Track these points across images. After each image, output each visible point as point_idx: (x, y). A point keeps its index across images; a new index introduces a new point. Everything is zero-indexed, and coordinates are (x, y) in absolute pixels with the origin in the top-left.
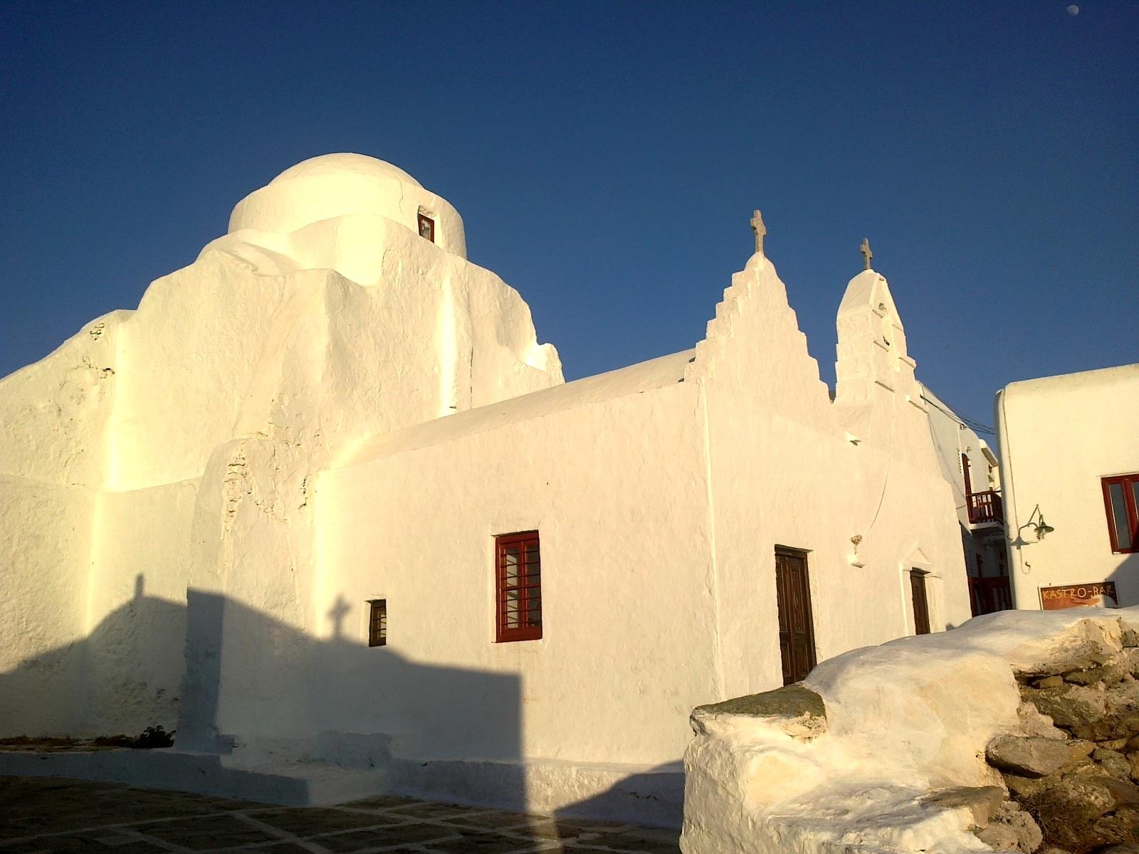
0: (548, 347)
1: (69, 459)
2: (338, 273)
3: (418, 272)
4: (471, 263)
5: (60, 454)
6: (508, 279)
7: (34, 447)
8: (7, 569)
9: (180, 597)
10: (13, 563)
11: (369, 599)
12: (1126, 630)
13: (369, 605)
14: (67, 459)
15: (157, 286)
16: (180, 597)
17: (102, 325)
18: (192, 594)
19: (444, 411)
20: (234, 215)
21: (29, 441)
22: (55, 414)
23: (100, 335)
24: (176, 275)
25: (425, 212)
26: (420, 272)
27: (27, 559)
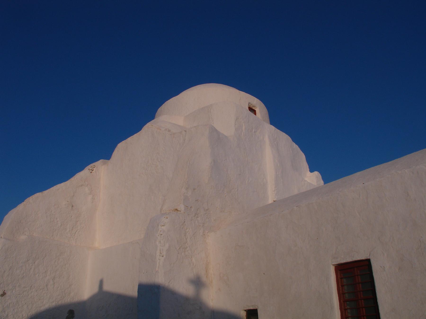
0: (316, 173)
1: (76, 231)
2: (214, 127)
3: (252, 131)
4: (277, 129)
5: (72, 229)
6: (295, 140)
7: (60, 225)
8: (44, 288)
9: (133, 292)
10: (47, 286)
11: (246, 309)
12: (1, 297)
13: (245, 312)
14: (75, 232)
15: (121, 146)
16: (133, 292)
17: (94, 166)
18: (67, 314)
19: (270, 201)
20: (160, 109)
21: (58, 221)
22: (71, 208)
23: (93, 171)
24: (129, 139)
25: (252, 106)
26: (253, 131)
27: (54, 283)
